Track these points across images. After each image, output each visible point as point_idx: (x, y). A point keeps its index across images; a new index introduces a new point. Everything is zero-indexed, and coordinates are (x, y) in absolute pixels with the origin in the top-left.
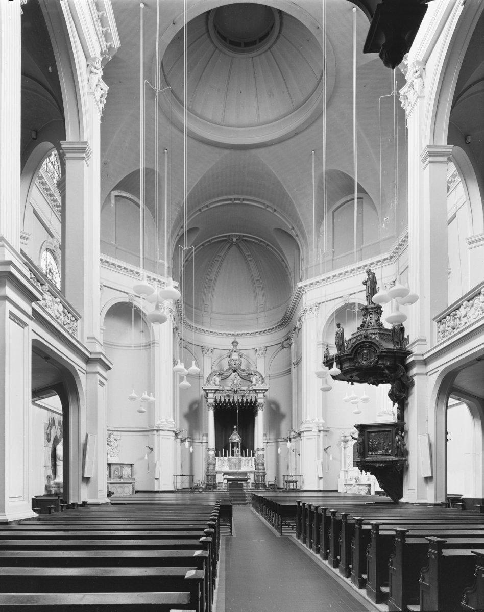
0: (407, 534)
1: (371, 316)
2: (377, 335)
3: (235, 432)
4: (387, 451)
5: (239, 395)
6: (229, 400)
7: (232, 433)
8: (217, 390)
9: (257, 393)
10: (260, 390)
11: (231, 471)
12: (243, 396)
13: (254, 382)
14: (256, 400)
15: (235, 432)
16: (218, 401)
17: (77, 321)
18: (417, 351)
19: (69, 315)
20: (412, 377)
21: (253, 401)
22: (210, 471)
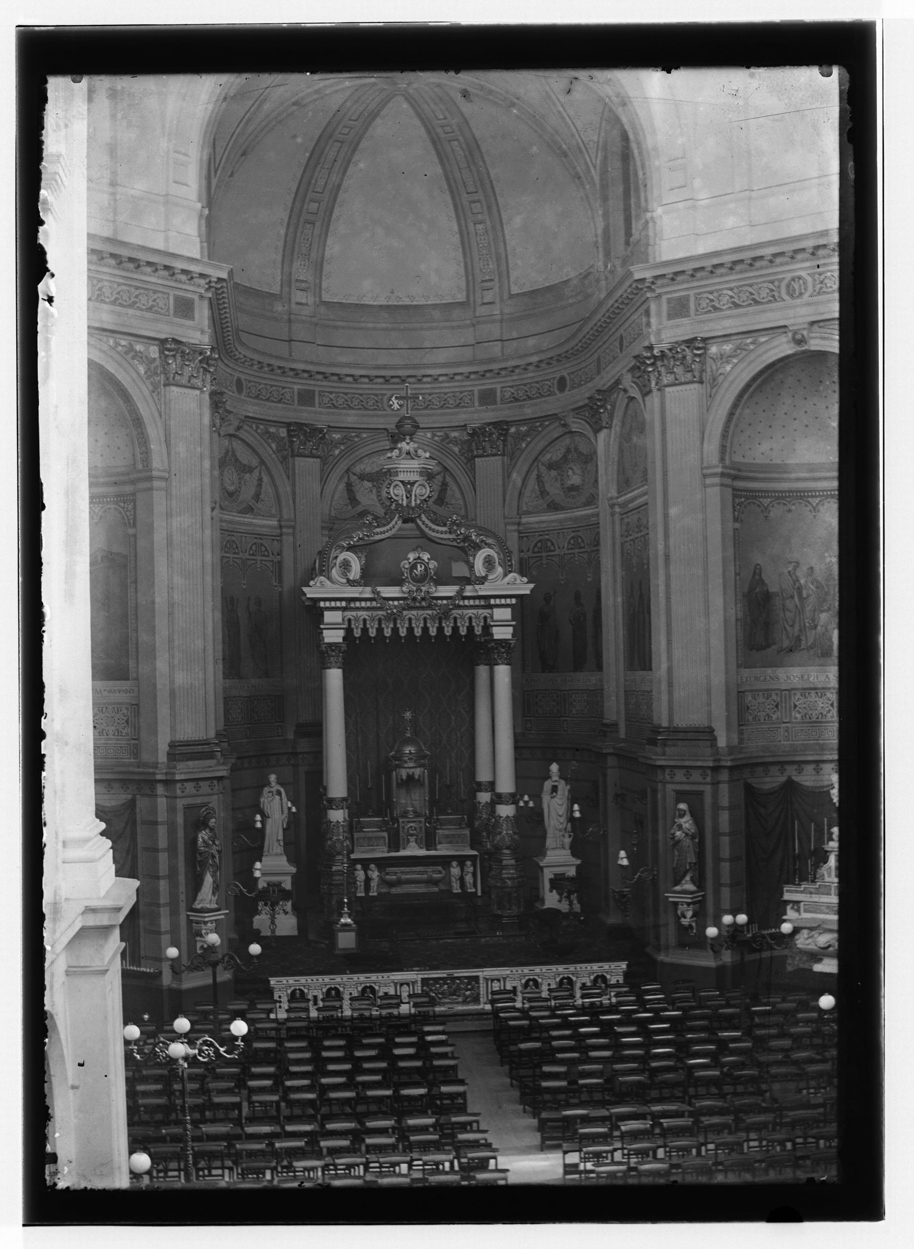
16: (357, 633)
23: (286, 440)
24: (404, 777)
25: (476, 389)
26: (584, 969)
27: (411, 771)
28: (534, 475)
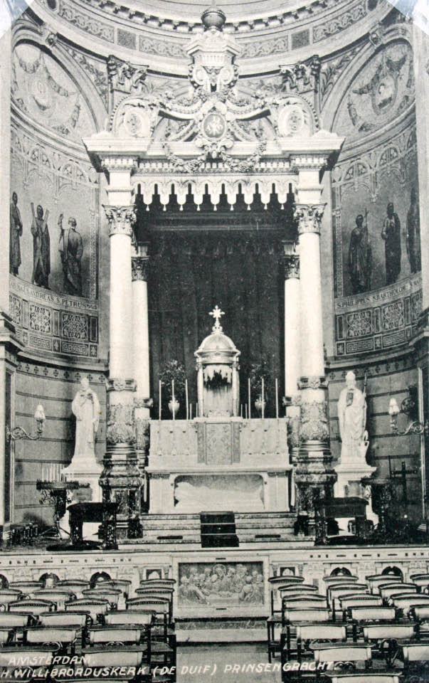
3: (217, 329)
11: (202, 467)
13: (284, 127)
14: (291, 197)
15: (217, 329)
16: (148, 200)
21: (282, 199)
22: (116, 470)
23: (106, 76)
24: (212, 376)
25: (290, 34)
26: (316, 557)
27: (217, 369)
28: (346, 101)
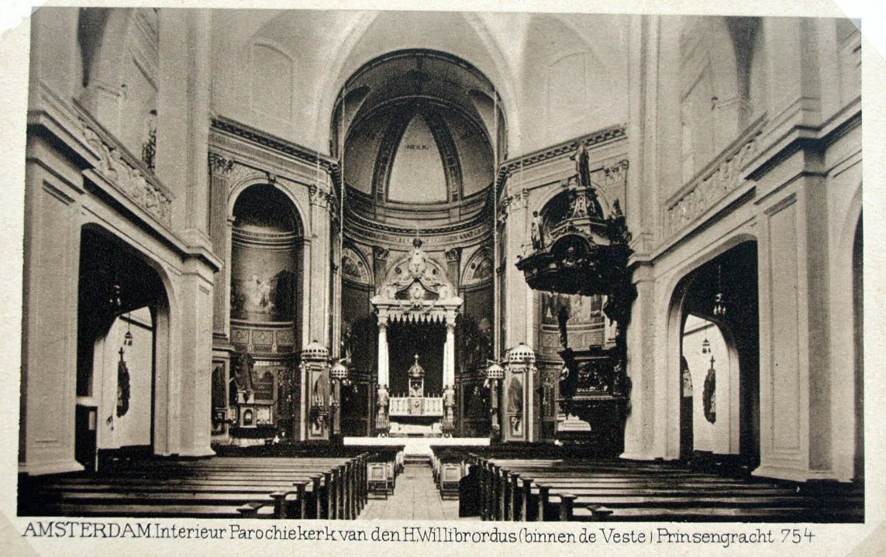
0: (575, 501)
1: (581, 201)
2: (588, 227)
4: (601, 387)
5: (421, 312)
6: (408, 319)
7: (414, 364)
8: (391, 305)
9: (446, 310)
10: (450, 306)
12: (427, 314)
14: (444, 319)
16: (392, 320)
17: (170, 202)
18: (639, 249)
19: (157, 194)
20: (635, 284)
21: (441, 320)
